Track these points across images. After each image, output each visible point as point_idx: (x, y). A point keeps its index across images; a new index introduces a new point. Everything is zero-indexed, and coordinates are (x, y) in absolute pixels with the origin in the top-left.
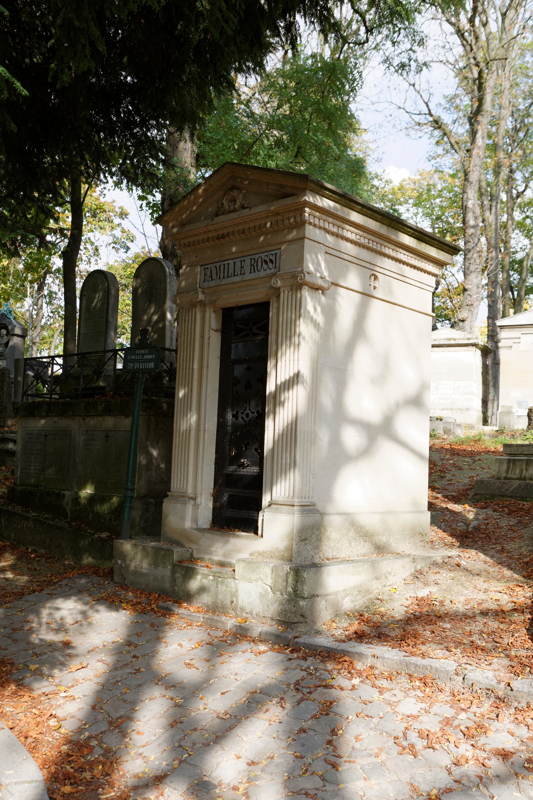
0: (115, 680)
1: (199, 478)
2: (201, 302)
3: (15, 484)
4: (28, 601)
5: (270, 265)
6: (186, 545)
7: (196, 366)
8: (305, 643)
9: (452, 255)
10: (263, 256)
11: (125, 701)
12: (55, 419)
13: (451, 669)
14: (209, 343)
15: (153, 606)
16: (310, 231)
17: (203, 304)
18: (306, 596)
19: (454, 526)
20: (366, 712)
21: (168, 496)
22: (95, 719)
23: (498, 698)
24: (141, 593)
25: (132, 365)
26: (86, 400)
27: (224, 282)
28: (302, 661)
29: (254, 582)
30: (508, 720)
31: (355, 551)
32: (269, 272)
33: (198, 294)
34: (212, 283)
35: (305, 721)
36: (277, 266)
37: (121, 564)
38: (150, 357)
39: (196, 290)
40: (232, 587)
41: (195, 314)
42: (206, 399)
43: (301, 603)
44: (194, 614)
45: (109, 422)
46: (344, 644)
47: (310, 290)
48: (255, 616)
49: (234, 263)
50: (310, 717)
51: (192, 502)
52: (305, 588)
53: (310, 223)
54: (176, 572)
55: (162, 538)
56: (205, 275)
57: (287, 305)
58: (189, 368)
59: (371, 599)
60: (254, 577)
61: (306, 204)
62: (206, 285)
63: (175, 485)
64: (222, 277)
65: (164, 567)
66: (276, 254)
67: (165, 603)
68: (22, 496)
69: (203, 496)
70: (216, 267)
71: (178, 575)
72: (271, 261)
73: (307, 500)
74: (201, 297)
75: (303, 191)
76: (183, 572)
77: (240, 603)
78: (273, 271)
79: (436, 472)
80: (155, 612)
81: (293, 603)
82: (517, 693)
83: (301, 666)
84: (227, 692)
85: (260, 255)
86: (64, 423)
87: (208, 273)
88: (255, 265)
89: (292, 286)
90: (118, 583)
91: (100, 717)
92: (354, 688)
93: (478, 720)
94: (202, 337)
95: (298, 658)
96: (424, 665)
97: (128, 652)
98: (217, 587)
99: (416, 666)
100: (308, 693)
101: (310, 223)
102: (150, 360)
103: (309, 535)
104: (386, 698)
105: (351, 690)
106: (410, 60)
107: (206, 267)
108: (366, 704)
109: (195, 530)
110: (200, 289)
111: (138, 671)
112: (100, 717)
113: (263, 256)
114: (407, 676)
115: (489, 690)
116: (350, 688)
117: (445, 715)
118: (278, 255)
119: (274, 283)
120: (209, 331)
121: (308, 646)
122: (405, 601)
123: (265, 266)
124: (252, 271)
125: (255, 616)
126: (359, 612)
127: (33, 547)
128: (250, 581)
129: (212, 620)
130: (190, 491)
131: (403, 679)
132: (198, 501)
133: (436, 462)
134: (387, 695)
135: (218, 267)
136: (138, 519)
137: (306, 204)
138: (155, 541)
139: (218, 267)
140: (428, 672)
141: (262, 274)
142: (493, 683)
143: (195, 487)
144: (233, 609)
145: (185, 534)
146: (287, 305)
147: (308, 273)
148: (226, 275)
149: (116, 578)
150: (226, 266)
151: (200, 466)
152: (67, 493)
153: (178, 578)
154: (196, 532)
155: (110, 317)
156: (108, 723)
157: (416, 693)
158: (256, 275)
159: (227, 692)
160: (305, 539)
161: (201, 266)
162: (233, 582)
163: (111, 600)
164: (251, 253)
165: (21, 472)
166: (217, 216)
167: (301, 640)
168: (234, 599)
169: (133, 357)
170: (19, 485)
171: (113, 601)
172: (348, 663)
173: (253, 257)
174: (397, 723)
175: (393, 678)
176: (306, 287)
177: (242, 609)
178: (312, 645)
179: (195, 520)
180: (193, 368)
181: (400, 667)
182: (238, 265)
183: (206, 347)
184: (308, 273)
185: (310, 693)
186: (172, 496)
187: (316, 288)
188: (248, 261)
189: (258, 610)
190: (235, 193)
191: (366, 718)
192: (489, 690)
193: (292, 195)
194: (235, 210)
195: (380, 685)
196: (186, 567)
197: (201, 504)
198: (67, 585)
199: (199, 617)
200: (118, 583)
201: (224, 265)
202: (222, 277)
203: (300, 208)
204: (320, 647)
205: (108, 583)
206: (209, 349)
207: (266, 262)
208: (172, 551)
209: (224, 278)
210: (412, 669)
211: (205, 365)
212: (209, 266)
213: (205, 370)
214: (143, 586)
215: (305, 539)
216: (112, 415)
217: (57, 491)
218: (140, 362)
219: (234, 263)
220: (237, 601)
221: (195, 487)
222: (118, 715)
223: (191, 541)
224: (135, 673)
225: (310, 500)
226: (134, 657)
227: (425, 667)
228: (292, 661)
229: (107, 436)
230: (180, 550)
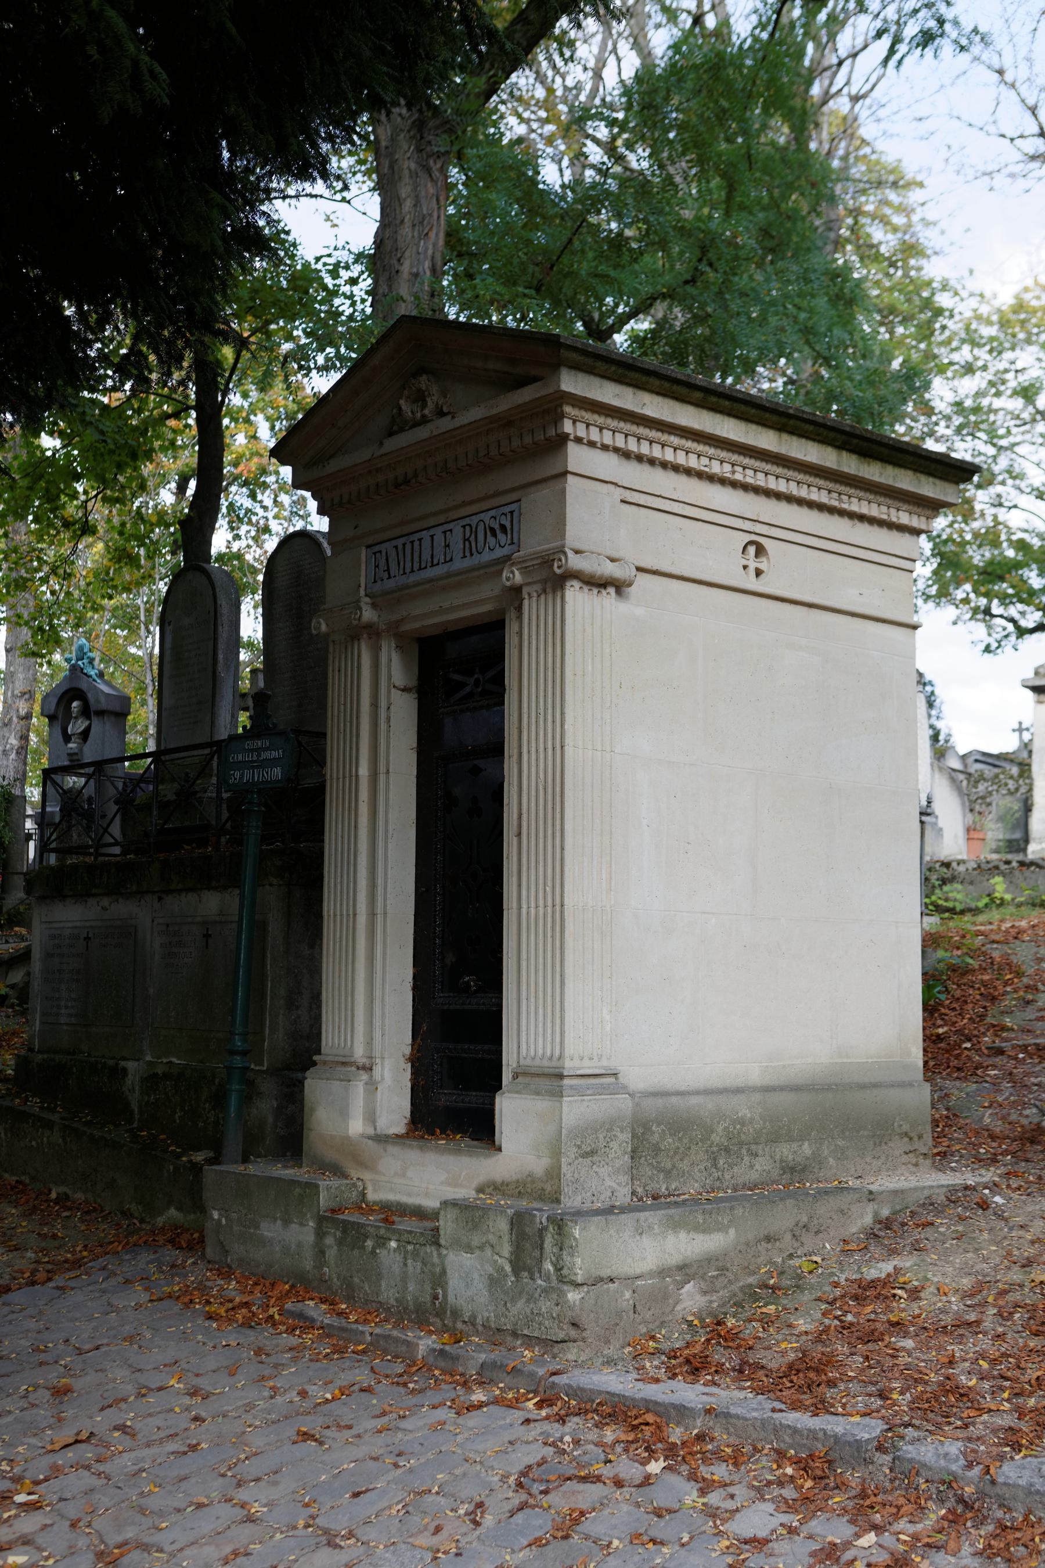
0: (137, 1467)
1: (377, 1022)
2: (369, 626)
3: (31, 1050)
4: (9, 1304)
5: (501, 536)
6: (354, 1174)
7: (364, 771)
8: (570, 1386)
9: (957, 483)
10: (486, 517)
11: (142, 1511)
12: (105, 902)
13: (867, 1436)
14: (388, 719)
15: (272, 1310)
16: (577, 457)
17: (372, 632)
18: (579, 1279)
19: (1014, 1117)
20: (653, 1533)
21: (314, 1064)
22: (70, 1547)
23: (961, 1500)
24: (256, 1284)
25: (237, 774)
26: (162, 856)
27: (413, 578)
28: (556, 1425)
29: (477, 1252)
30: (971, 1550)
31: (727, 1176)
32: (499, 553)
33: (361, 609)
35: (513, 1551)
36: (515, 540)
37: (219, 1220)
38: (274, 754)
39: (358, 601)
40: (433, 1265)
41: (359, 656)
42: (386, 843)
43: (570, 1296)
44: (354, 1326)
45: (211, 903)
46: (654, 1386)
47: (586, 589)
48: (480, 1328)
49: (432, 536)
50: (526, 1543)
51: (365, 1077)
52: (578, 1261)
53: (579, 440)
54: (325, 1234)
55: (304, 1160)
56: (377, 566)
57: (538, 626)
58: (351, 776)
59: (750, 1286)
60: (476, 1240)
61: (562, 397)
62: (378, 587)
63: (330, 1040)
64: (408, 570)
65: (301, 1224)
66: (512, 512)
67: (300, 1305)
68: (39, 1075)
69: (387, 1062)
70: (396, 547)
71: (329, 1241)
72: (503, 528)
73: (595, 1063)
74: (368, 614)
75: (555, 367)
76: (338, 1234)
77: (451, 1298)
78: (506, 551)
79: (1015, 991)
80: (274, 1325)
81: (555, 1296)
82: (1005, 1488)
83: (549, 1435)
84: (367, 1491)
85: (482, 516)
86: (123, 909)
87: (382, 563)
89: (544, 582)
90: (215, 1262)
91: (82, 1543)
92: (647, 1481)
93: (902, 1548)
94: (375, 705)
95: (547, 1418)
96: (809, 1430)
97: (188, 1409)
98: (405, 1265)
99: (795, 1431)
100: (541, 1492)
101: (579, 440)
102: (273, 762)
103: (602, 1143)
104: (712, 1502)
105: (639, 1486)
106: (941, 22)
107: (376, 549)
108: (660, 1516)
109: (369, 1138)
110: (367, 600)
111: (194, 1448)
112: (82, 1543)
114: (775, 1456)
115: (943, 1482)
116: (638, 1482)
117: (829, 1539)
118: (515, 514)
119: (508, 579)
120: (389, 692)
121: (574, 1392)
122: (828, 1288)
123: (491, 540)
125: (480, 1328)
126: (716, 1317)
127: (63, 1189)
128: (469, 1249)
129: (387, 1337)
130: (359, 1053)
131: (764, 1462)
132: (377, 1071)
133: (1024, 968)
134: (714, 1498)
135: (400, 547)
136: (270, 1119)
137: (562, 397)
138: (293, 1167)
139: (400, 547)
140: (820, 1446)
141: (487, 557)
142: (954, 1467)
143: (369, 1043)
144: (437, 1315)
145: (349, 1147)
146: (538, 626)
147: (577, 552)
148: (416, 566)
149: (209, 1252)
150: (416, 544)
151: (378, 993)
152: (131, 1065)
153: (330, 1247)
154: (370, 1142)
155: (220, 667)
156: (96, 1554)
157: (783, 1491)
158: (476, 560)
159: (367, 1491)
160: (593, 1153)
161: (368, 547)
162: (435, 1253)
163: (186, 1300)
164: (463, 512)
165: (42, 1023)
166: (391, 434)
167: (561, 1380)
169: (240, 757)
170: (39, 1052)
171: (191, 1301)
172: (652, 1428)
174: (713, 1555)
175: (741, 1460)
176: (577, 584)
178: (583, 1390)
179: (371, 1117)
180: (357, 776)
181: (762, 1434)
182: (439, 538)
183: (383, 726)
184: (577, 552)
185: (545, 1492)
186: (325, 1063)
187: (598, 583)
188: (458, 531)
189: (486, 1314)
190: (423, 381)
191: (651, 1545)
192: (950, 1483)
193: (535, 379)
194: (424, 421)
195: (708, 1476)
196: (344, 1221)
197: (383, 1079)
198: (104, 1268)
199: (363, 1332)
200: (215, 1262)
202: (408, 570)
203: (555, 406)
204: (600, 1392)
205: (194, 1263)
206: (389, 731)
208: (317, 1186)
209: (412, 571)
210: (787, 1439)
211: (382, 768)
212: (383, 547)
213: (382, 778)
214: (262, 1267)
215: (593, 1153)
216: (215, 889)
217: (111, 1062)
218: (253, 767)
219: (432, 536)
220: (445, 1295)
221: (369, 1043)
222: (120, 1539)
223: (362, 1164)
224: (185, 1453)
225: (604, 1063)
226: (196, 1419)
227: (812, 1434)
228: (532, 1425)
229: (207, 936)
230: (335, 1183)
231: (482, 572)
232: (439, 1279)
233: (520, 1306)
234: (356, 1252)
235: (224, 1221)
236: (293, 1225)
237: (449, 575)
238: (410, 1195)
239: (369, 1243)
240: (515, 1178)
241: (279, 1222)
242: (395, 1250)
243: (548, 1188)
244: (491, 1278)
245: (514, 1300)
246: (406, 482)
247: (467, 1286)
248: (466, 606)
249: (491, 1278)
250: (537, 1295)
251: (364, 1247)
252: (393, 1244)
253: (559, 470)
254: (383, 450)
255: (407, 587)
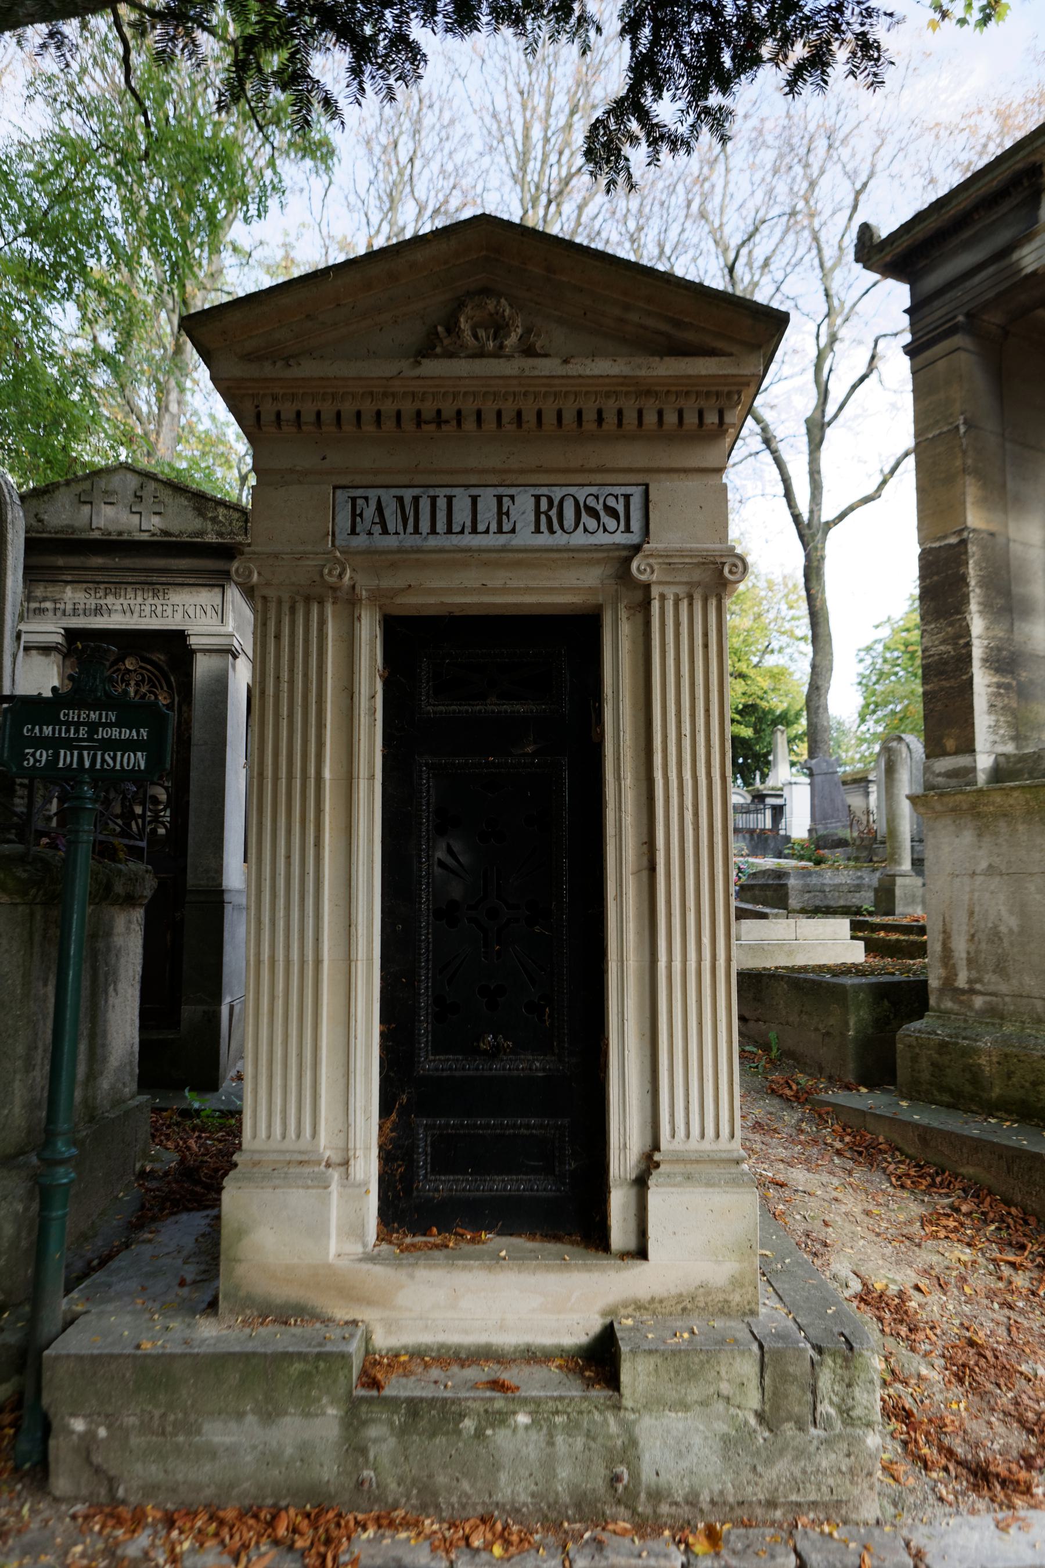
25: (43, 756)
34: (390, 542)
54: (364, 1423)
60: (694, 1393)
70: (400, 500)
72: (613, 513)
77: (647, 1475)
85: (572, 490)
88: (553, 513)
109: (360, 1260)
113: (581, 494)
123: (591, 523)
124: (543, 527)
128: (683, 1406)
135: (408, 501)
150: (442, 503)
162: (612, 1421)
168: (622, 1470)
173: (544, 491)
177: (656, 1496)
186: (257, 1164)
189: (717, 1487)
201: (434, 500)
207: (593, 513)
218: (80, 749)
220: (635, 1475)
231: (565, 555)
232: (629, 1450)
233: (781, 1469)
234: (440, 1440)
235: (102, 1432)
236: (288, 1419)
237: (504, 549)
238: (466, 1332)
239: (468, 1424)
240: (674, 1291)
241: (251, 1418)
242: (527, 1428)
243: (736, 1298)
244: (725, 1439)
245: (769, 1462)
246: (439, 419)
247: (680, 1455)
248: (528, 590)
249: (725, 1439)
250: (812, 1449)
251: (458, 1432)
252: (523, 1419)
253: (711, 462)
254: (417, 372)
255: (419, 550)
